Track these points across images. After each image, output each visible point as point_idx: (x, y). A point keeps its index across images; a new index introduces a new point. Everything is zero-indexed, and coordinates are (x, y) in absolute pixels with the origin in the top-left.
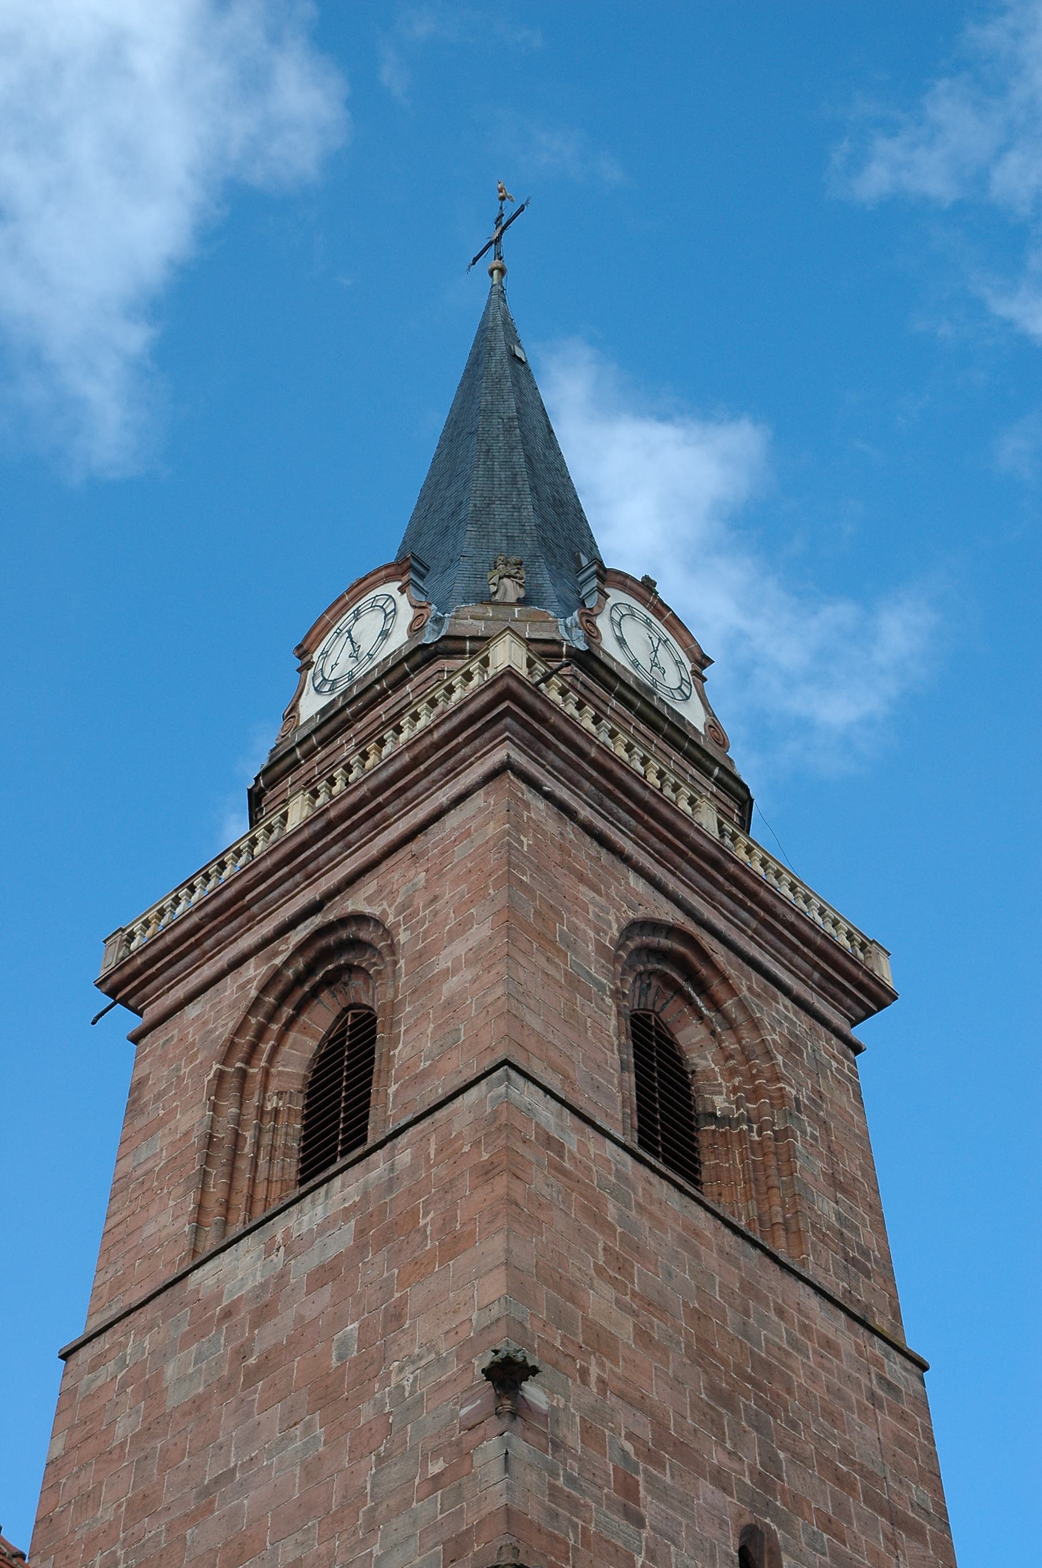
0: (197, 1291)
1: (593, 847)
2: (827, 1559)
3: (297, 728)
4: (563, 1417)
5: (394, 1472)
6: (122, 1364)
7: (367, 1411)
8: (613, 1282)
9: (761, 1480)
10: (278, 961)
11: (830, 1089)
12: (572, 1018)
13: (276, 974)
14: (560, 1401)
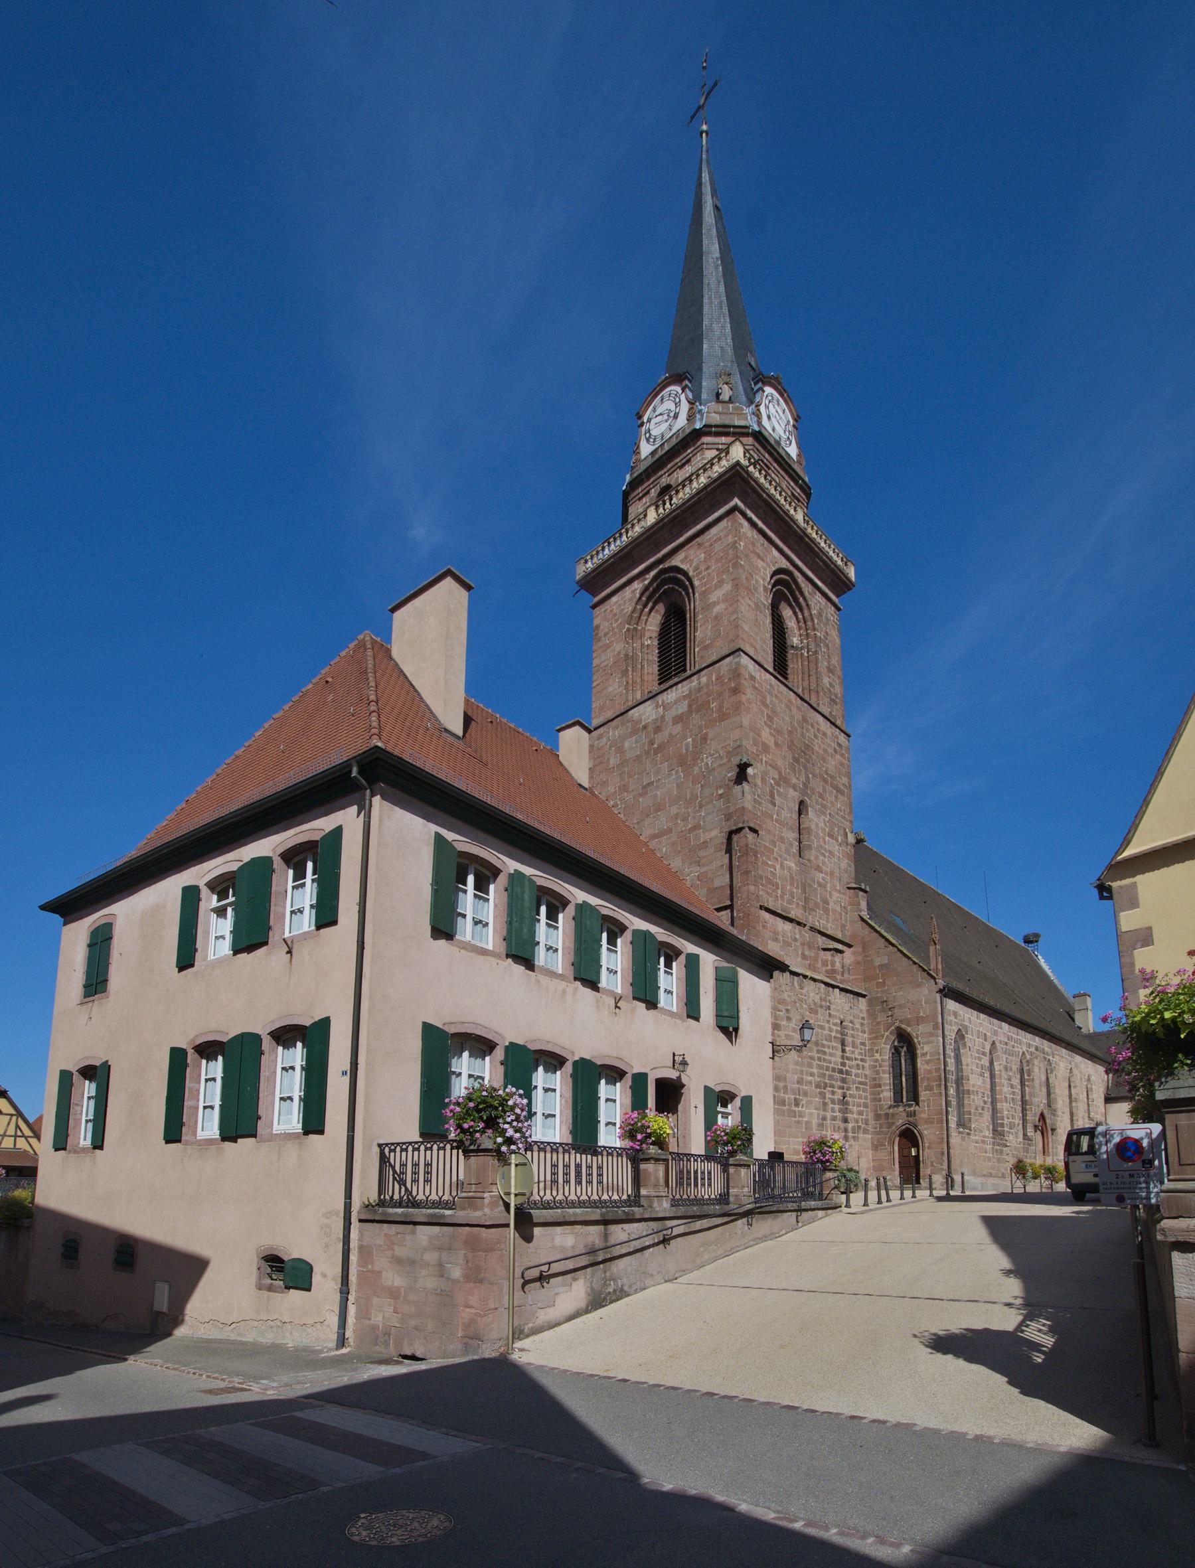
1: (762, 540)
5: (707, 791)
6: (608, 739)
7: (696, 770)
9: (805, 785)
10: (646, 582)
13: (646, 589)
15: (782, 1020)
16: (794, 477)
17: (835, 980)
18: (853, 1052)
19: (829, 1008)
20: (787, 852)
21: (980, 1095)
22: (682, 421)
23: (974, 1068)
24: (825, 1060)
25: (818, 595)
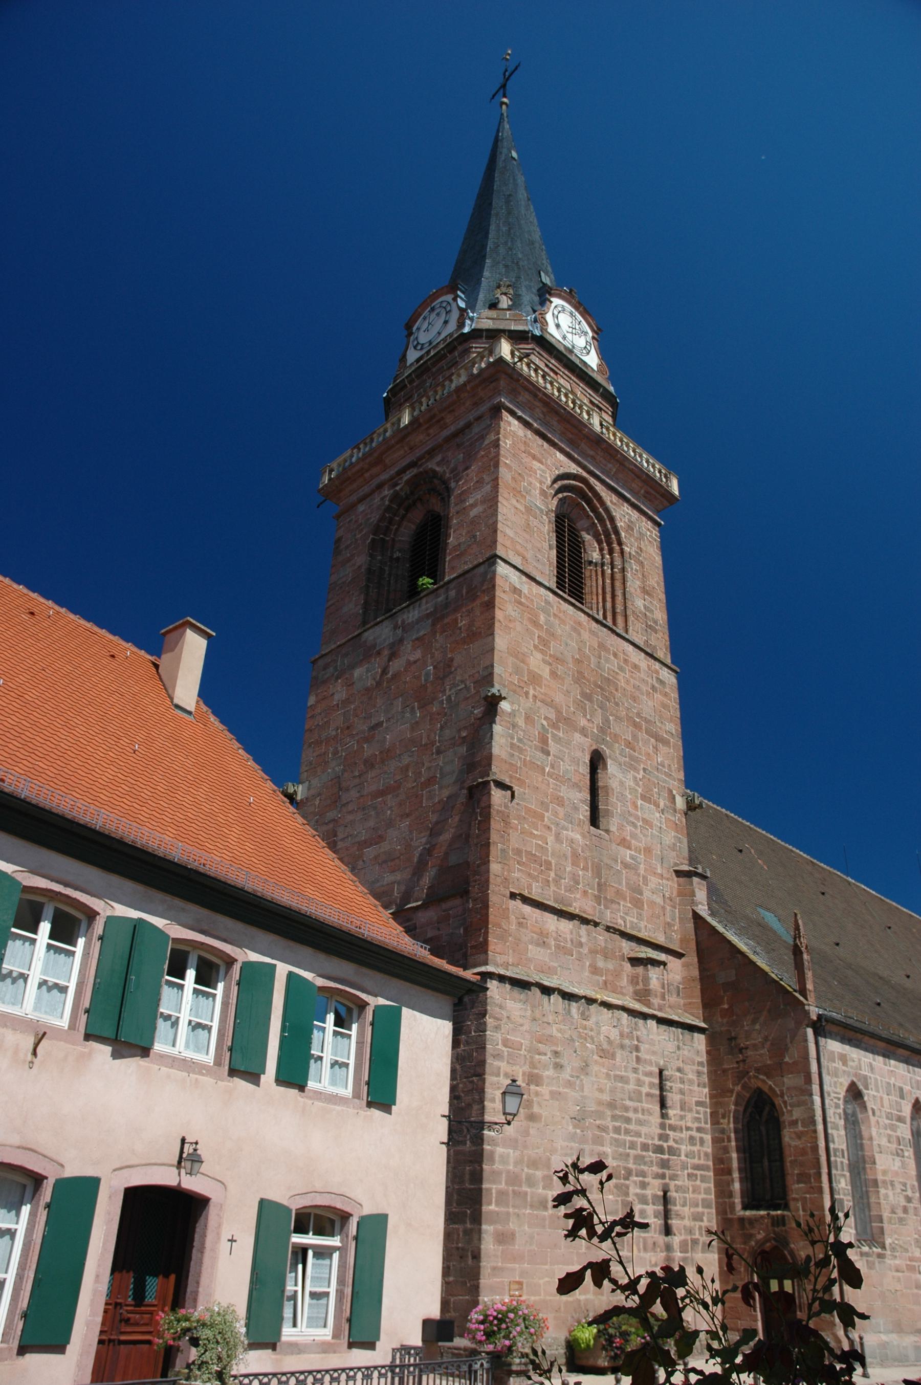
0: (365, 641)
2: (627, 759)
3: (406, 367)
4: (517, 714)
8: (542, 652)
9: (602, 730)
11: (646, 546)
12: (528, 528)
14: (516, 707)
15: (545, 1067)
16: (593, 384)
17: (648, 1004)
18: (682, 1118)
19: (637, 1049)
20: (568, 818)
21: (899, 1187)
22: (452, 327)
23: (884, 1142)
24: (627, 1132)
25: (626, 508)
